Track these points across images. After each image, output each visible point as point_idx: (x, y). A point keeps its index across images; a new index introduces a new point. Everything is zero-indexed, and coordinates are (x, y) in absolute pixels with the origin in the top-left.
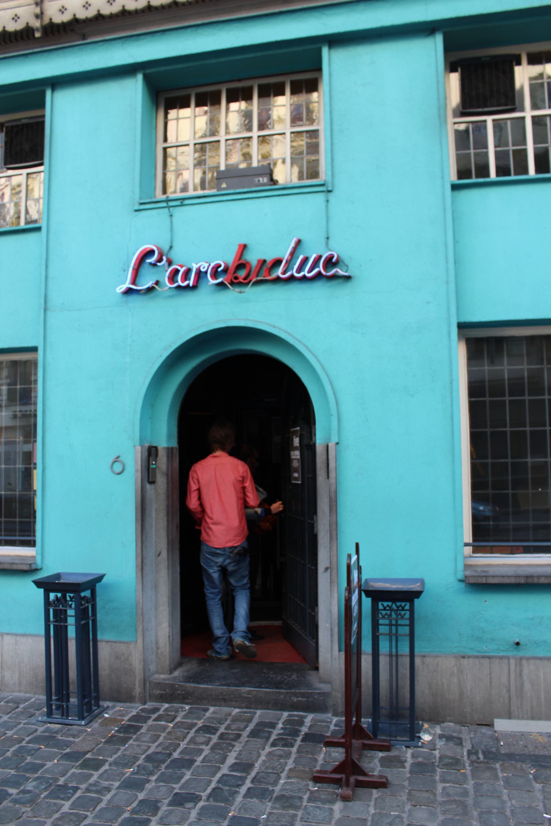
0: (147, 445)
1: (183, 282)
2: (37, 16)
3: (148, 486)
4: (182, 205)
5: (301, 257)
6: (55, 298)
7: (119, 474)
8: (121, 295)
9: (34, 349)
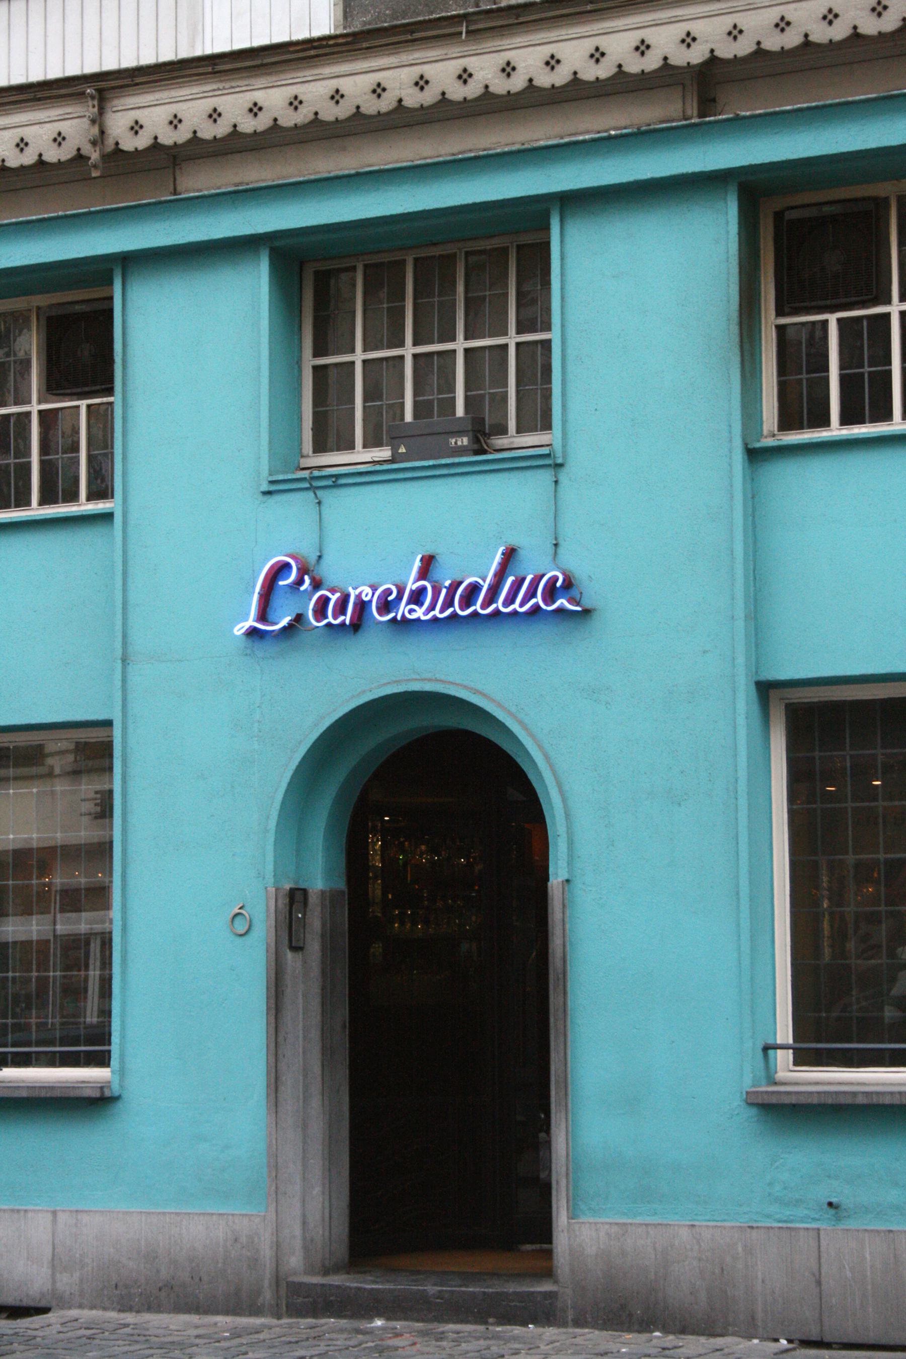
0: (287, 886)
1: (335, 617)
2: (94, 143)
3: (289, 955)
4: (336, 486)
5: (511, 579)
6: (140, 641)
7: (241, 935)
8: (244, 638)
9: (108, 724)
